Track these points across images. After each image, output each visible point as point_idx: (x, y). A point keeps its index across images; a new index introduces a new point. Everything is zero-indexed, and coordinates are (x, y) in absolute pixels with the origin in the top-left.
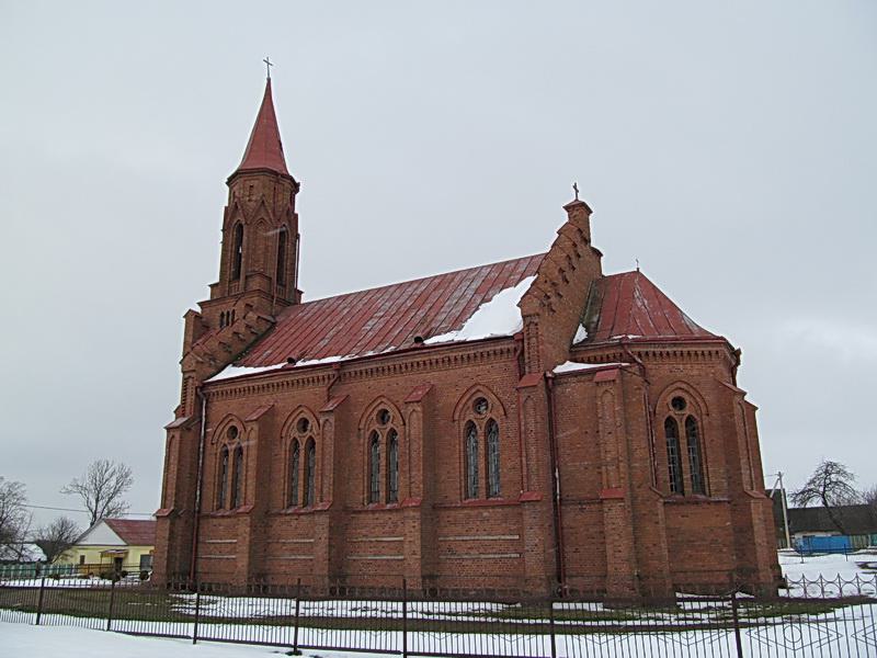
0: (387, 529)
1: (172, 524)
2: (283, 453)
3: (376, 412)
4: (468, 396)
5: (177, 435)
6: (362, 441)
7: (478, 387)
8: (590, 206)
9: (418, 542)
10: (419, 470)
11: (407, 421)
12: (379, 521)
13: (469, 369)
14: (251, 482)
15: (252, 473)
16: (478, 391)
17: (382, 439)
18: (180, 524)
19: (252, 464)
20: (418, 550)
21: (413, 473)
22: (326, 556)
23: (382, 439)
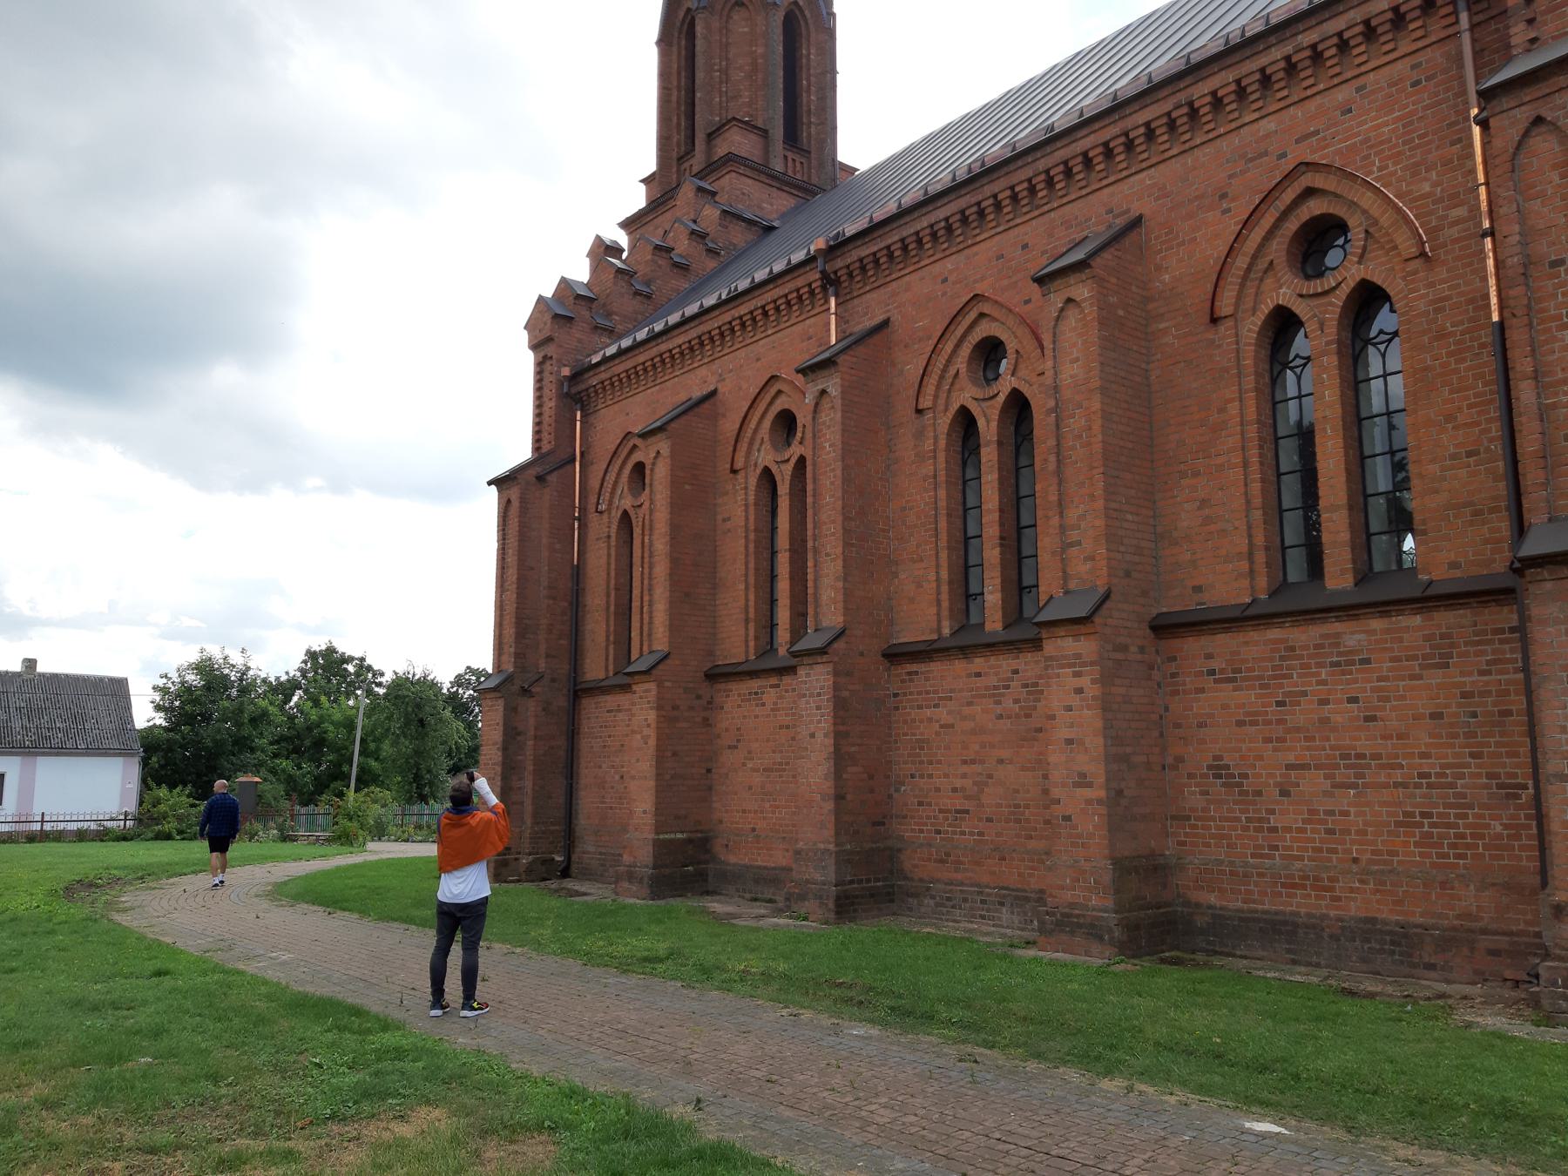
0: (1008, 704)
1: (511, 711)
2: (740, 512)
3: (966, 350)
4: (1267, 222)
5: (514, 494)
6: (928, 445)
7: (1308, 180)
8: (1327, 562)
9: (1095, 743)
10: (1092, 497)
11: (1048, 344)
12: (981, 682)
13: (1269, 125)
14: (661, 594)
15: (661, 569)
16: (1309, 192)
17: (989, 427)
18: (530, 710)
19: (661, 545)
20: (1098, 772)
21: (1072, 514)
22: (828, 786)
23: (989, 427)
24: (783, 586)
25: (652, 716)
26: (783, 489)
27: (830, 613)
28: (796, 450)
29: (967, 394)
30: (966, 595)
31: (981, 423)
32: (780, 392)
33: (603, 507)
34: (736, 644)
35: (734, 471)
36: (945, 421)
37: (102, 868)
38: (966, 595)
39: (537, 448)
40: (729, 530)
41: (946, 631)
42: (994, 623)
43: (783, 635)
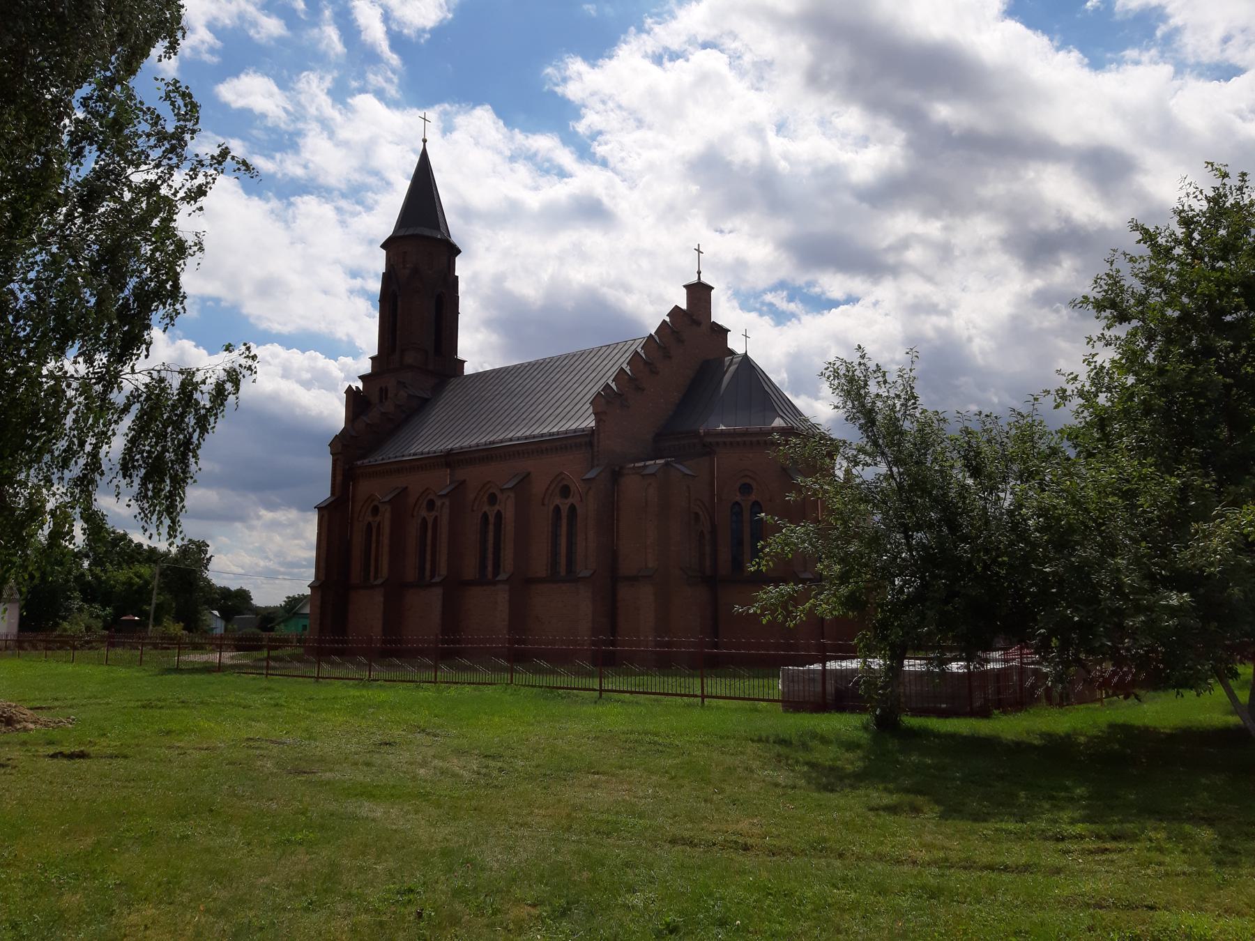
17: (564, 513)
24: (428, 557)
25: (382, 599)
26: (430, 526)
27: (443, 570)
28: (497, 507)
29: (486, 508)
30: (483, 566)
31: (490, 517)
32: (563, 479)
33: (360, 519)
34: (540, 566)
35: (473, 511)
36: (552, 507)
37: (358, 769)
38: (483, 566)
39: (333, 493)
40: (212, 556)
41: (477, 577)
42: (563, 573)
43: (428, 573)
